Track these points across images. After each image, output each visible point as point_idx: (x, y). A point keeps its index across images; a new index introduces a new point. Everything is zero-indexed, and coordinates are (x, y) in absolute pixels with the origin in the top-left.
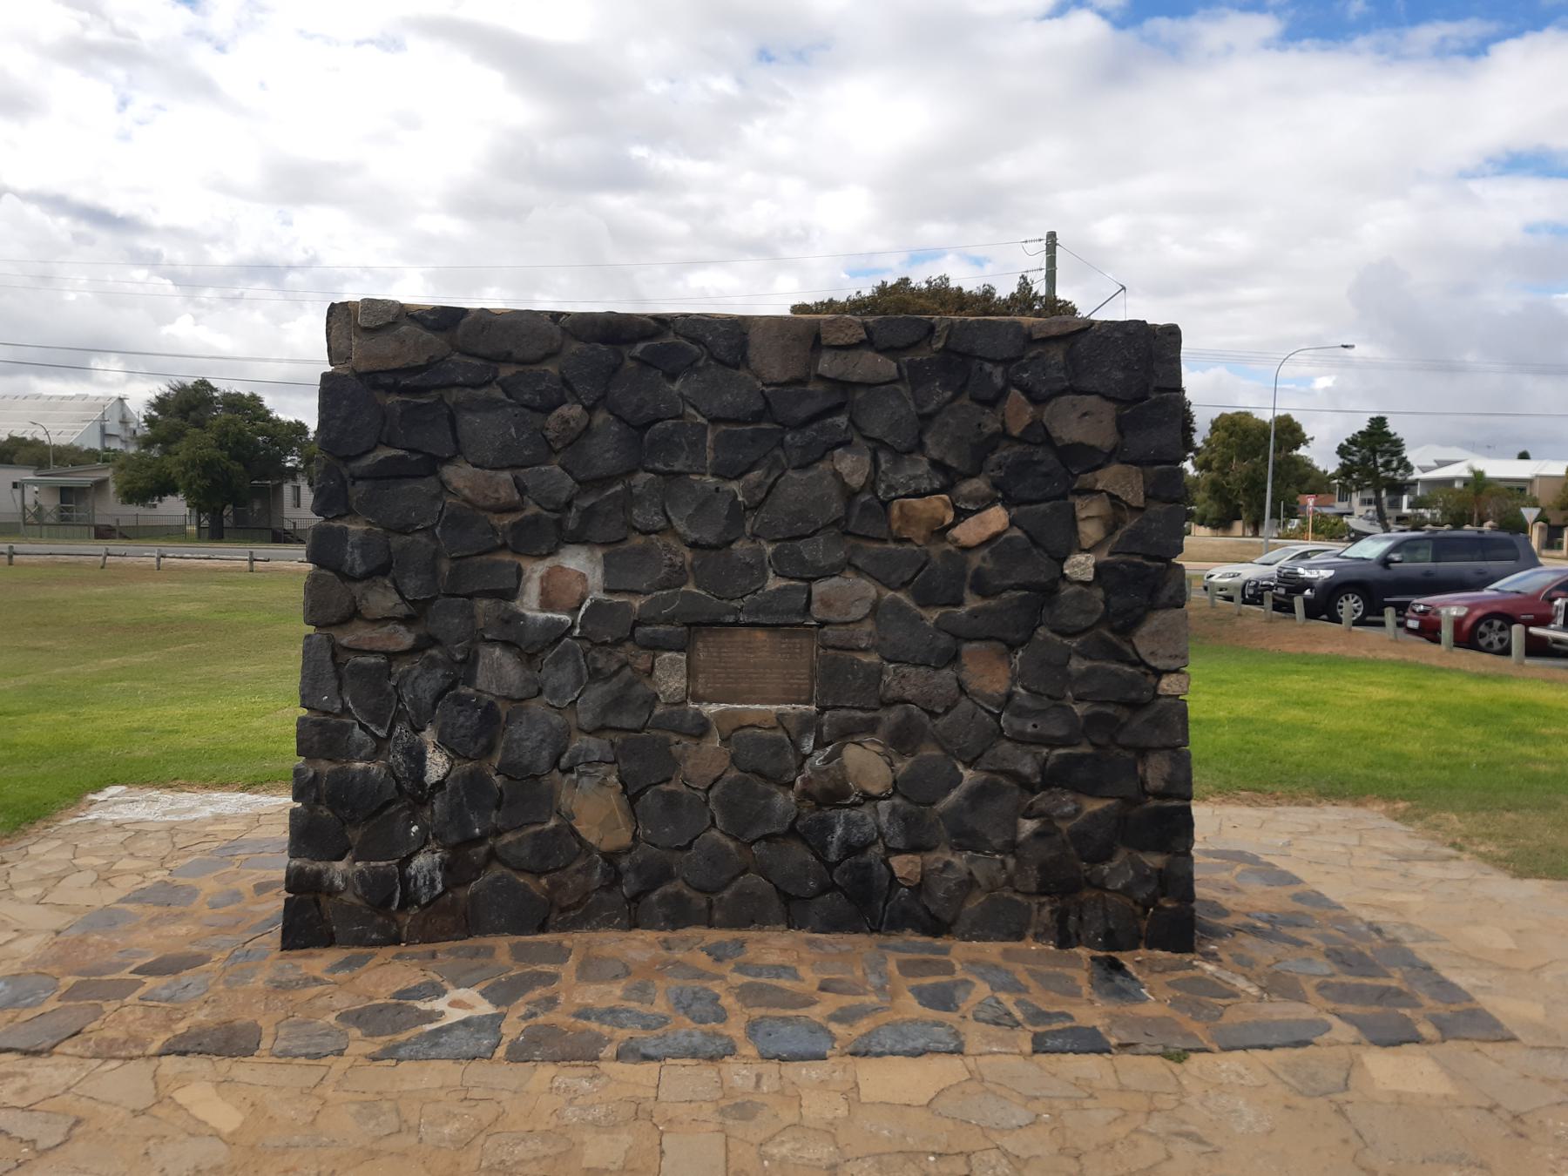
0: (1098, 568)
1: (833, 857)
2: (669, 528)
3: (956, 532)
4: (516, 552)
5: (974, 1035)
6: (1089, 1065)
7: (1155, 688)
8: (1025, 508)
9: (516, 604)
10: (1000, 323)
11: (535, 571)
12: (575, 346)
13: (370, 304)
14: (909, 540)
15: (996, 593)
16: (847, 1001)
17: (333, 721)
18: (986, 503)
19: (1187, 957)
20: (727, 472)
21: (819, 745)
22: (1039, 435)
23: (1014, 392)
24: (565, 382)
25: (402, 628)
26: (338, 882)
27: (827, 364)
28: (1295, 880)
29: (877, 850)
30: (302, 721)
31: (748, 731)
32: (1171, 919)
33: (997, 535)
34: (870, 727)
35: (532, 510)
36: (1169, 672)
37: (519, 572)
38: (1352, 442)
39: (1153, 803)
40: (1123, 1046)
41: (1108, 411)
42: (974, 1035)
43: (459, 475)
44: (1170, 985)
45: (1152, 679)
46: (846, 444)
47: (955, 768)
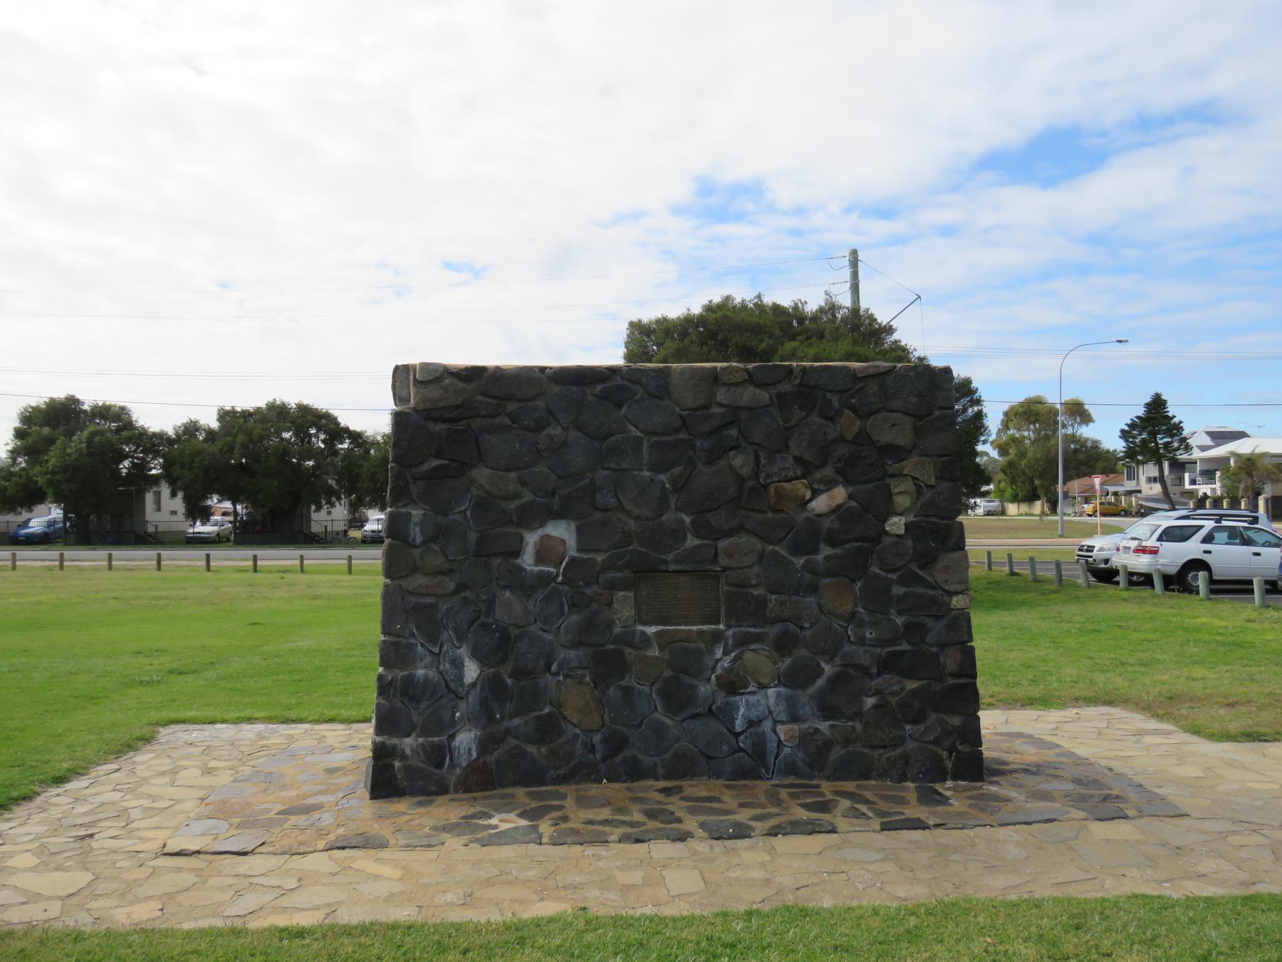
0: (908, 526)
1: (738, 729)
2: (621, 506)
3: (813, 504)
4: (518, 525)
5: (842, 824)
6: (917, 835)
7: (949, 604)
8: (858, 487)
9: (519, 561)
10: (835, 367)
11: (532, 539)
12: (556, 389)
13: (426, 367)
14: (781, 511)
15: (842, 543)
16: (759, 811)
17: (404, 641)
18: (829, 484)
19: (980, 784)
20: (658, 468)
21: (726, 653)
22: (863, 438)
23: (847, 411)
24: (550, 412)
25: (447, 579)
26: (408, 751)
27: (722, 395)
28: (1058, 746)
29: (767, 725)
30: (384, 642)
31: (678, 644)
32: (970, 764)
33: (839, 506)
34: (758, 638)
35: (528, 497)
36: (957, 593)
37: (522, 539)
38: (1133, 426)
39: (951, 681)
40: (937, 826)
41: (908, 423)
42: (842, 824)
43: (481, 475)
44: (968, 798)
45: (946, 598)
46: (736, 447)
47: (819, 665)
